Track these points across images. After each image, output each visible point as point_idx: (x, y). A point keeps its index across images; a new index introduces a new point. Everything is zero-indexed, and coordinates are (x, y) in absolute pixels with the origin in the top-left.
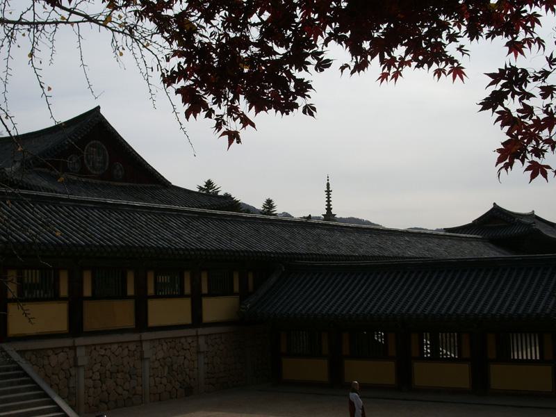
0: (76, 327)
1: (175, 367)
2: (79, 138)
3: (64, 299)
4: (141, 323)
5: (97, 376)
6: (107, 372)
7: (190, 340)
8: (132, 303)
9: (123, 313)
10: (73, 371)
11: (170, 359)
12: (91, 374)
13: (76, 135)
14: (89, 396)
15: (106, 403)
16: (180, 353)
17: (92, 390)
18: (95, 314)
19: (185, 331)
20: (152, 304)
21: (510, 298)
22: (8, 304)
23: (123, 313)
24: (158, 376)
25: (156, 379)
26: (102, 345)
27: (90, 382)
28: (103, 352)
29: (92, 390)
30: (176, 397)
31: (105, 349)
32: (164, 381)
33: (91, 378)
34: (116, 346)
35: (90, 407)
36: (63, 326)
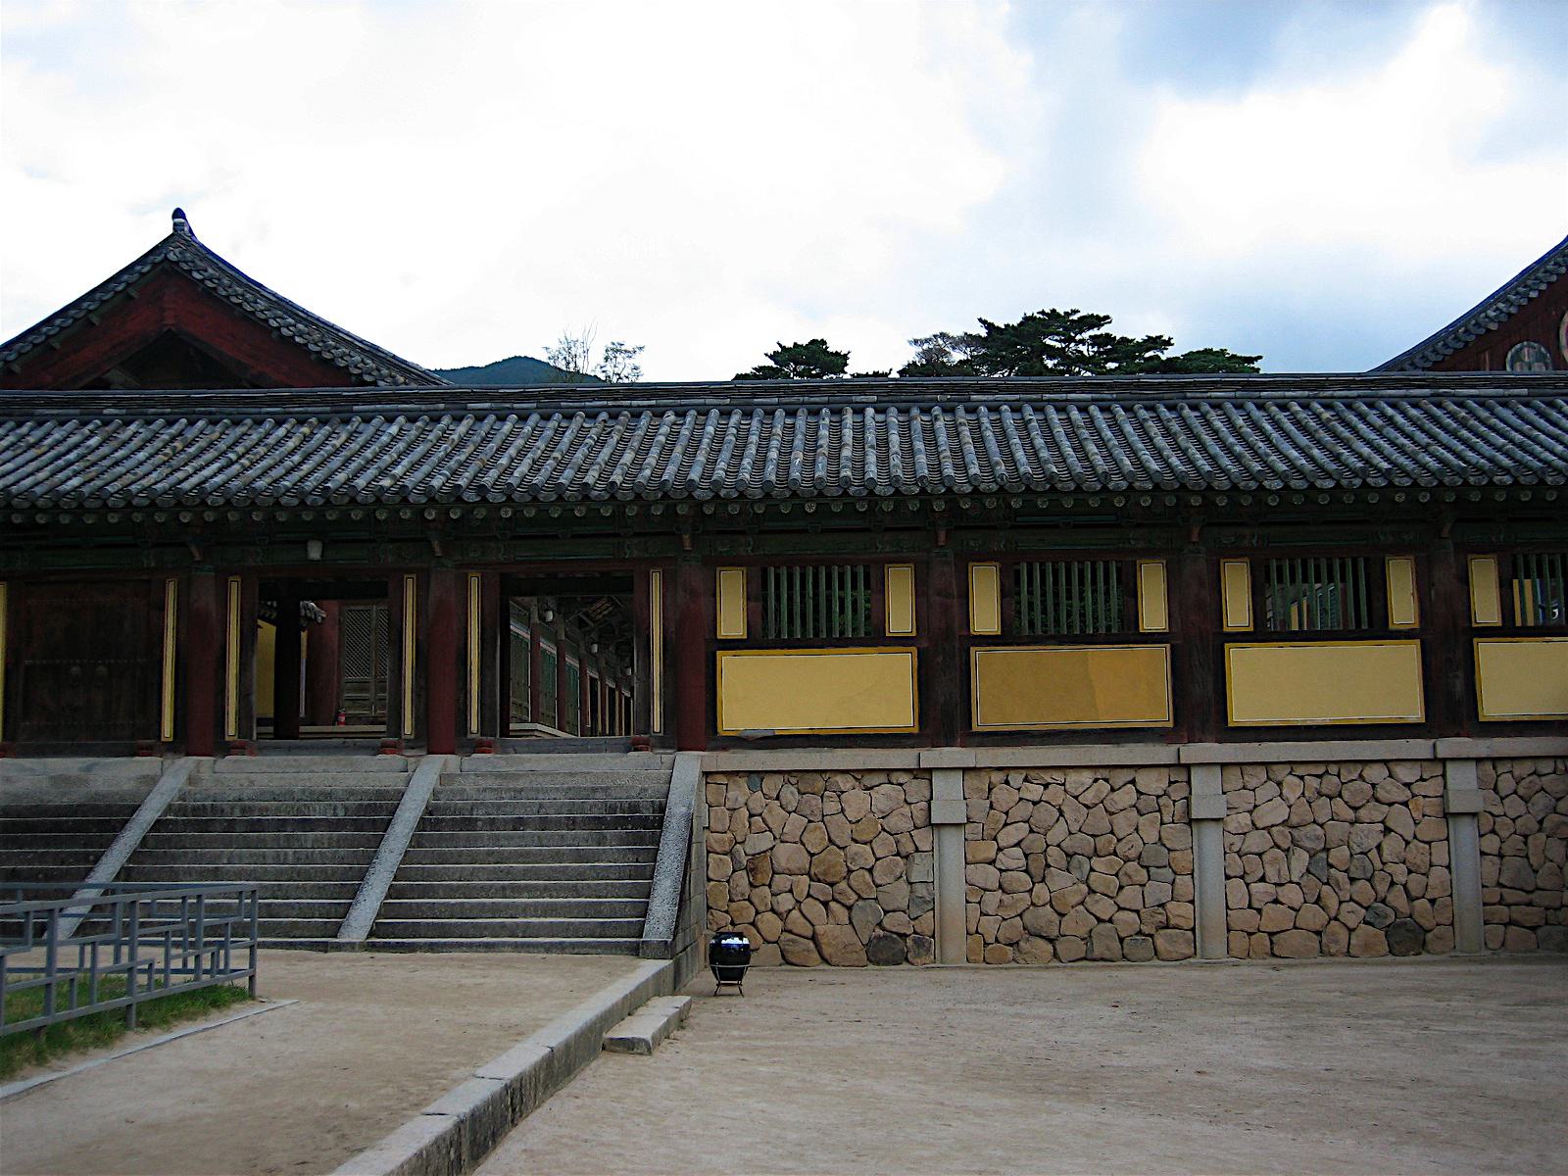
0: (944, 713)
1: (1339, 855)
2: (1533, 295)
3: (901, 641)
4: (1200, 706)
5: (1013, 858)
6: (1053, 851)
7: (1406, 774)
8: (1411, 650)
9: (1131, 683)
10: (923, 838)
11: (1320, 831)
12: (992, 854)
13: (1521, 289)
14: (982, 914)
15: (1051, 941)
16: (1362, 813)
17: (992, 900)
18: (1007, 684)
19: (840, 752)
20: (1240, 661)
21: (825, 450)
22: (719, 653)
23: (1131, 683)
24: (1263, 879)
25: (1256, 887)
26: (1029, 772)
27: (989, 876)
28: (1034, 791)
29: (992, 900)
30: (1348, 953)
31: (1046, 786)
32: (1292, 895)
33: (992, 862)
34: (1087, 777)
35: (986, 944)
36: (902, 715)
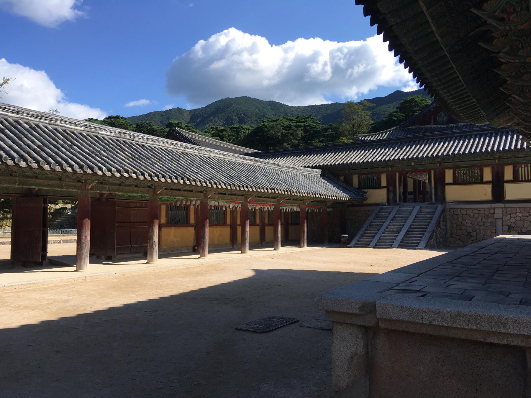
3: (383, 187)
